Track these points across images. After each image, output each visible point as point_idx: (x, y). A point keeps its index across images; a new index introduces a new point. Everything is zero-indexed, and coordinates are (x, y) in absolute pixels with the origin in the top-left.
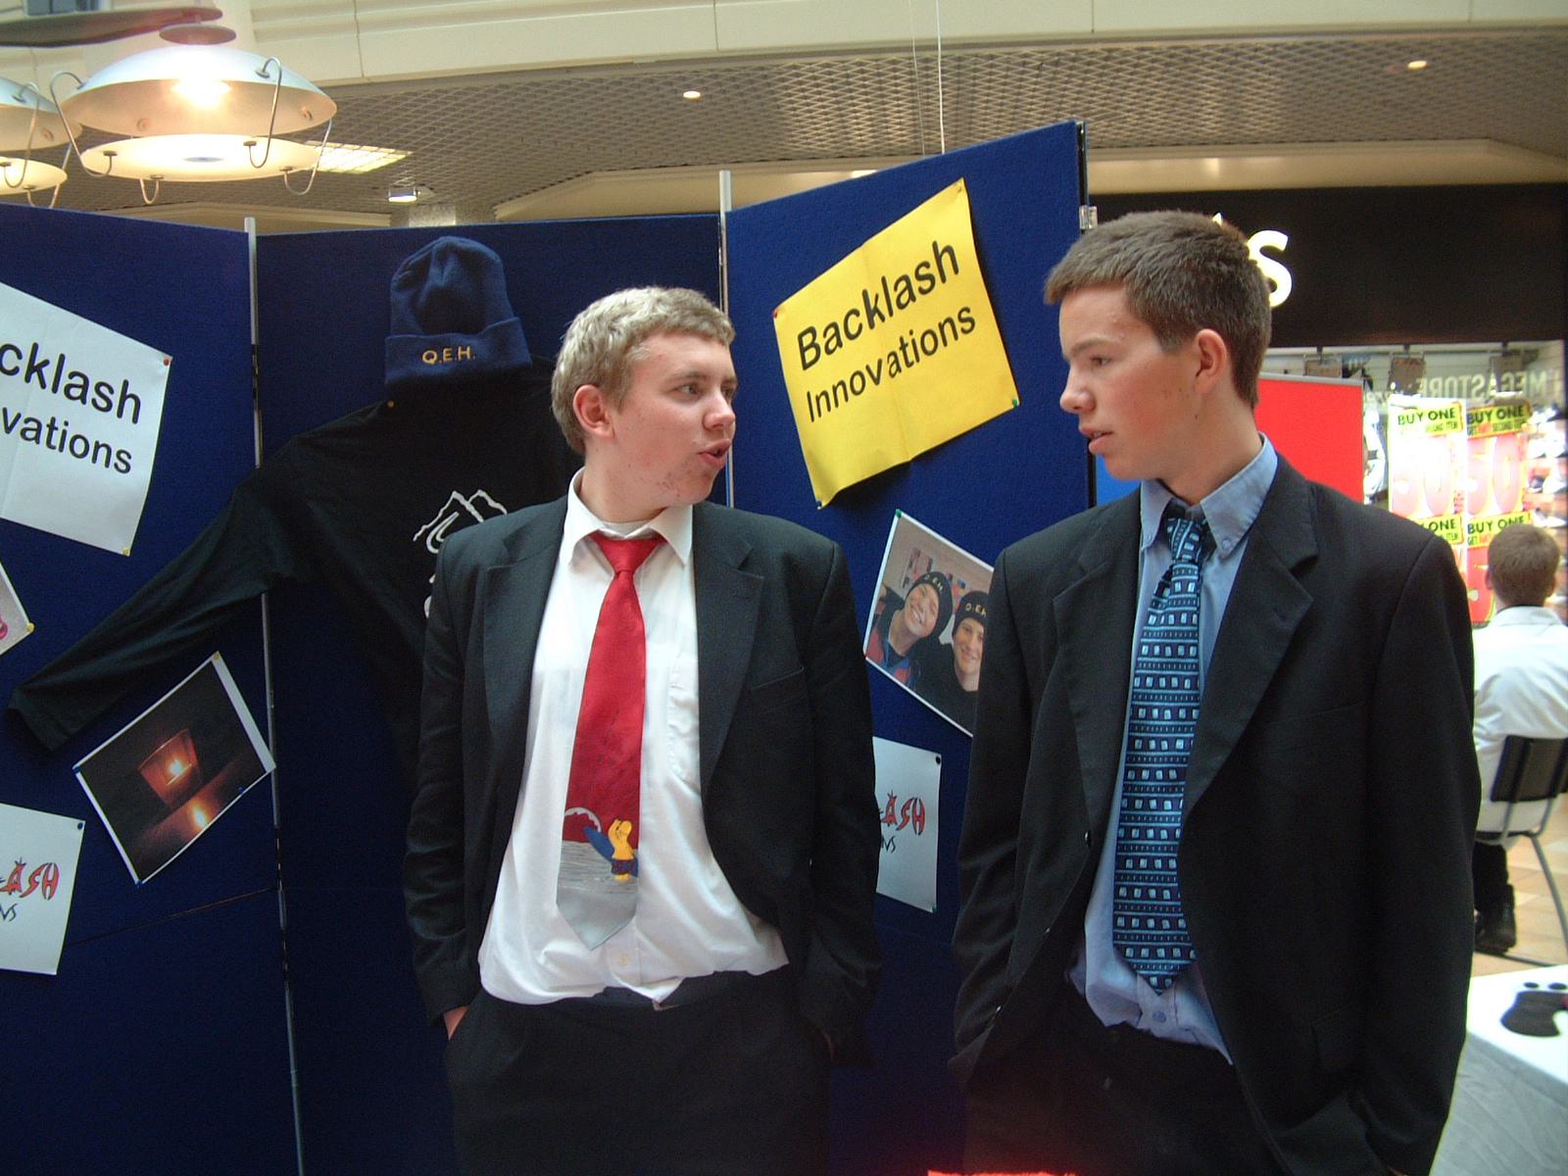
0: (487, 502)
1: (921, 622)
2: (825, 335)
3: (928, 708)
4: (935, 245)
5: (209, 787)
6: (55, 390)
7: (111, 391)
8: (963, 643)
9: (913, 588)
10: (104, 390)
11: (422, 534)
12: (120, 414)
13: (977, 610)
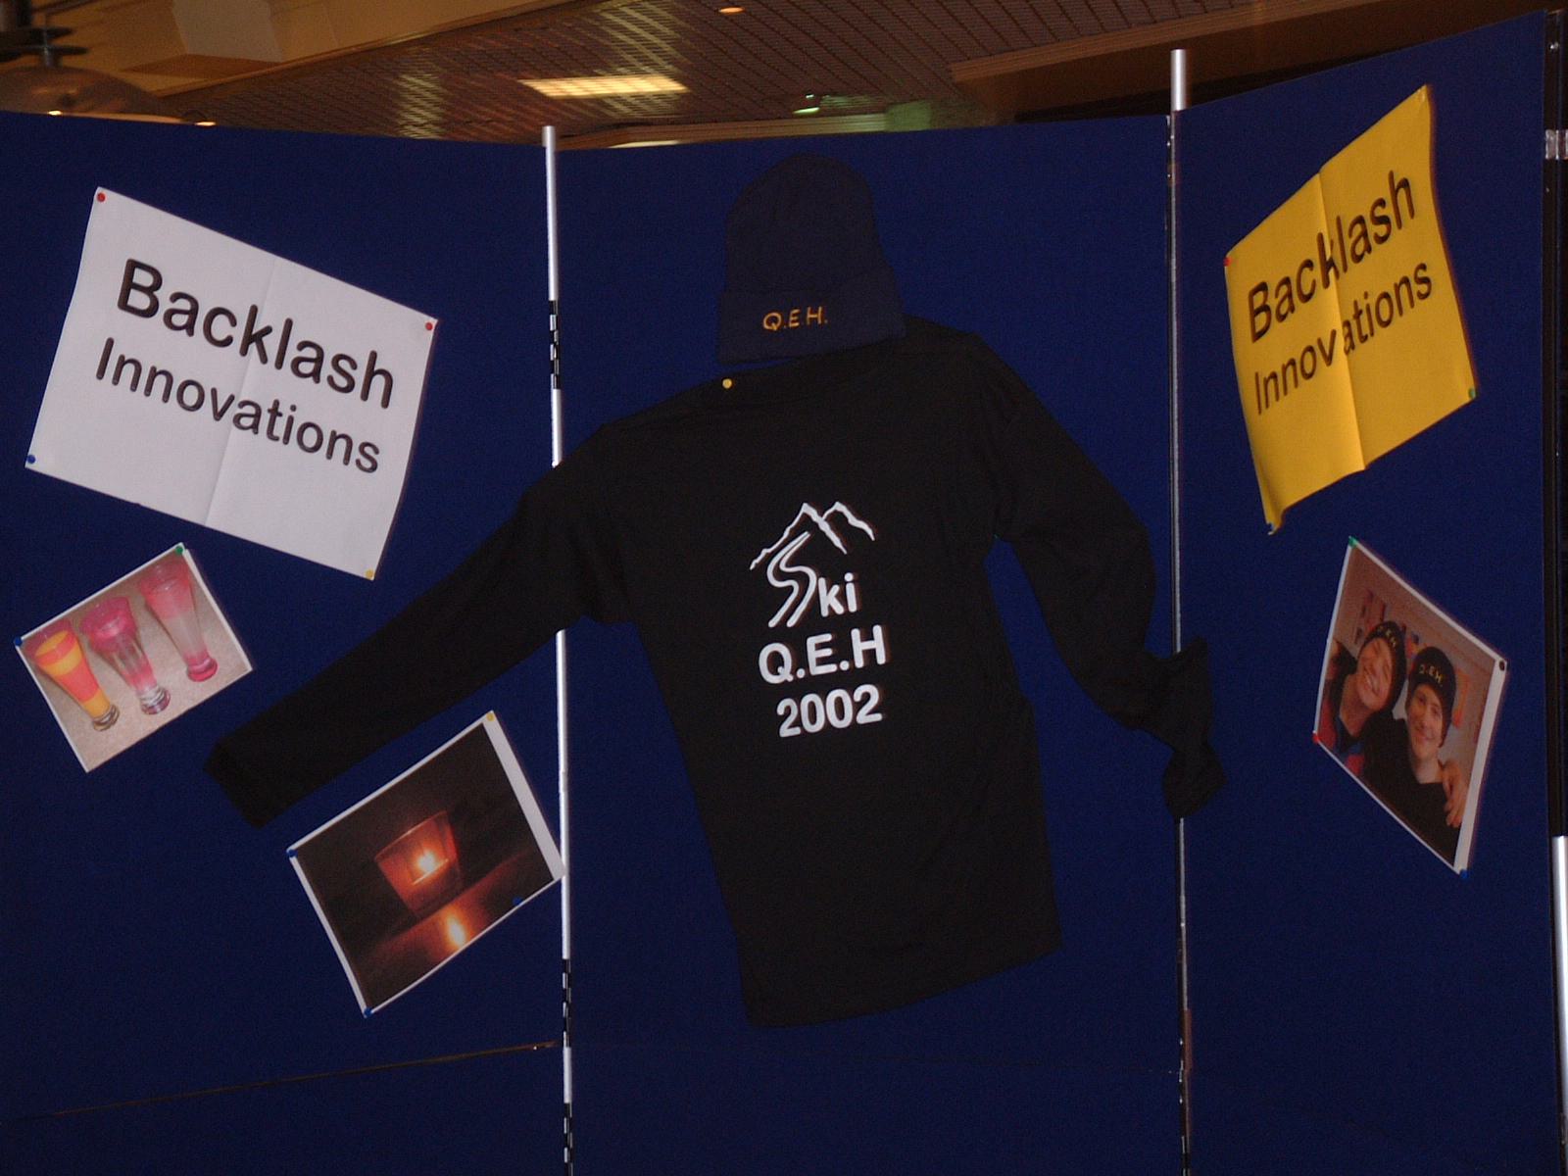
0: (846, 519)
4: (1391, 176)
6: (279, 364)
7: (354, 366)
8: (1416, 717)
10: (344, 364)
12: (365, 396)
13: (1431, 673)
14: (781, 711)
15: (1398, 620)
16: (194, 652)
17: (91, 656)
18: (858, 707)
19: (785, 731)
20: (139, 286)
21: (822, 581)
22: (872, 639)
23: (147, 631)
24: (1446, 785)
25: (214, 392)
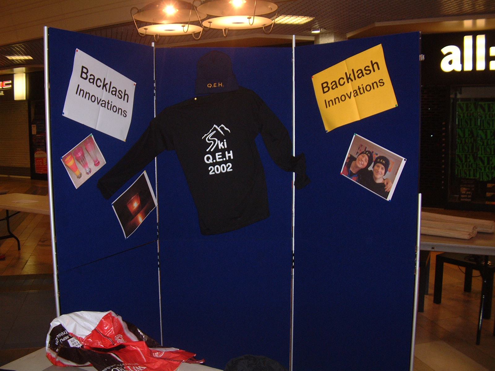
0: (224, 128)
1: (362, 164)
2: (331, 84)
3: (125, 193)
4: (372, 62)
9: (359, 155)
11: (205, 137)
14: (209, 169)
15: (371, 151)
17: (76, 161)
18: (227, 168)
19: (211, 173)
20: (84, 71)
21: (219, 141)
22: (230, 153)
23: (86, 155)
24: (385, 183)
25: (347, 94)
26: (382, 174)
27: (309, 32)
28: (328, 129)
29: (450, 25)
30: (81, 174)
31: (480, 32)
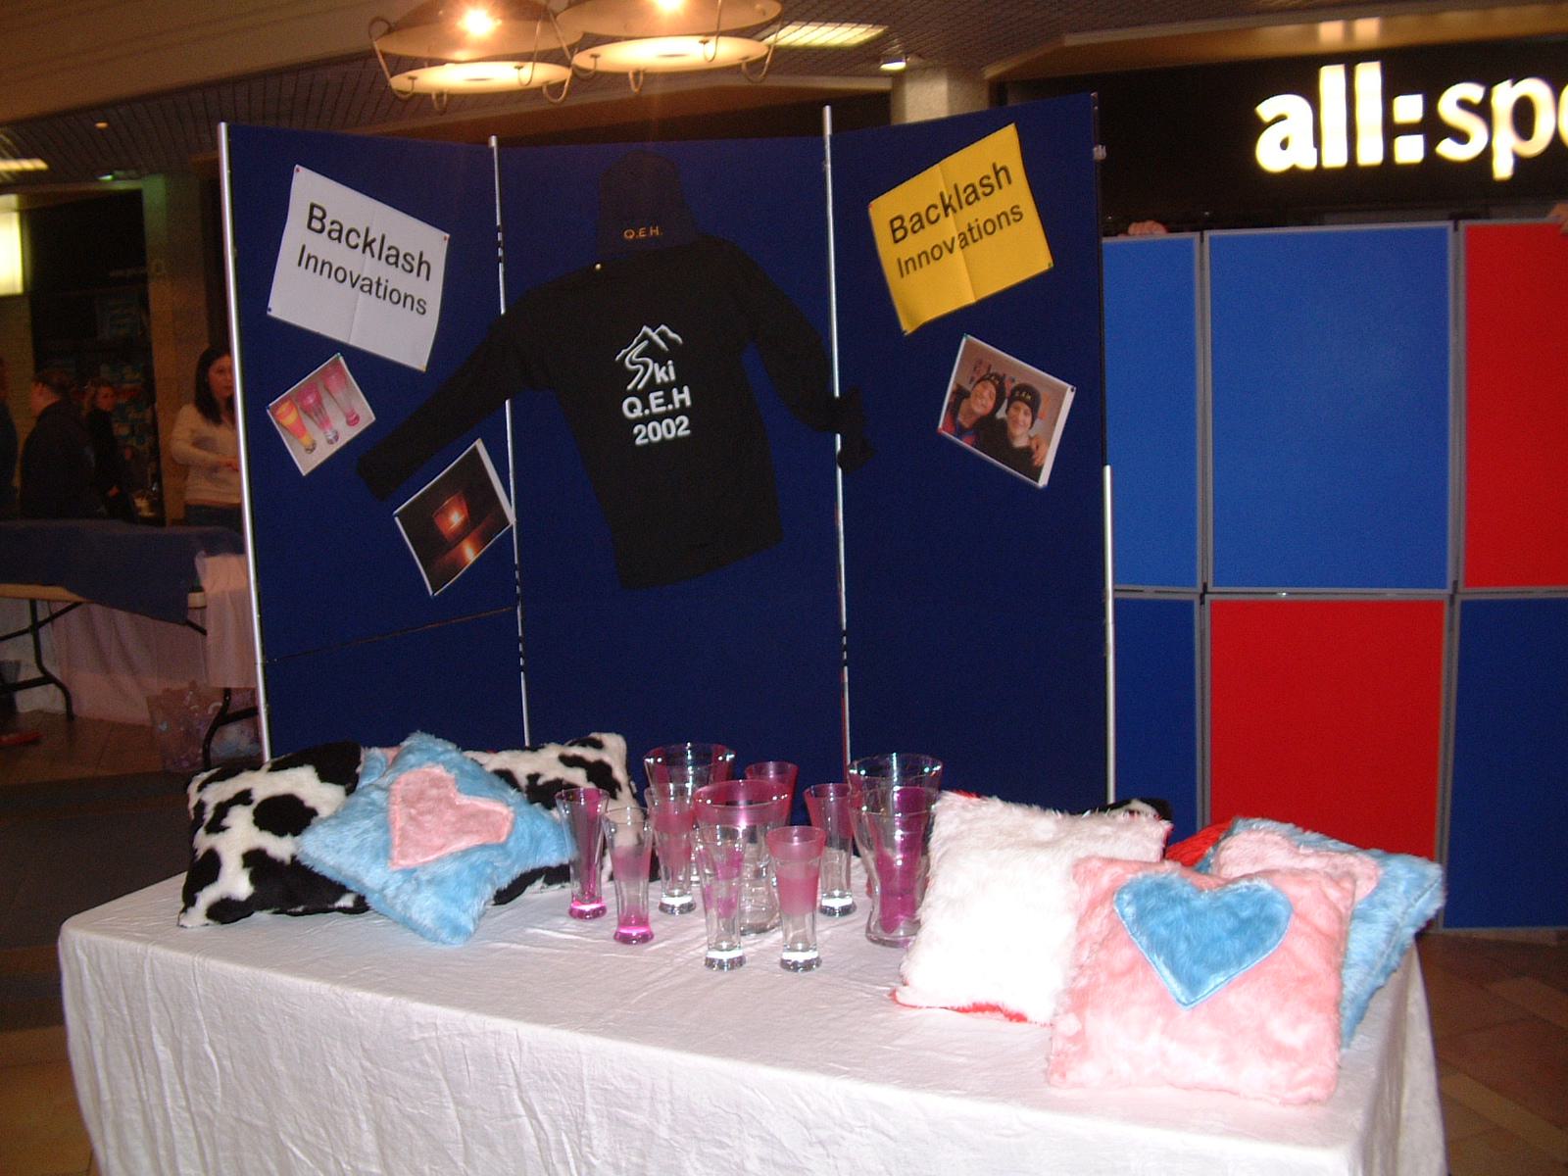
4: (994, 166)
5: (473, 533)
6: (380, 258)
14: (636, 431)
15: (1001, 373)
16: (348, 411)
17: (301, 413)
18: (678, 427)
19: (639, 441)
21: (656, 365)
24: (1034, 447)
26: (1025, 425)
27: (872, 67)
28: (907, 327)
29: (1279, 39)
30: (314, 445)
31: (1367, 55)
